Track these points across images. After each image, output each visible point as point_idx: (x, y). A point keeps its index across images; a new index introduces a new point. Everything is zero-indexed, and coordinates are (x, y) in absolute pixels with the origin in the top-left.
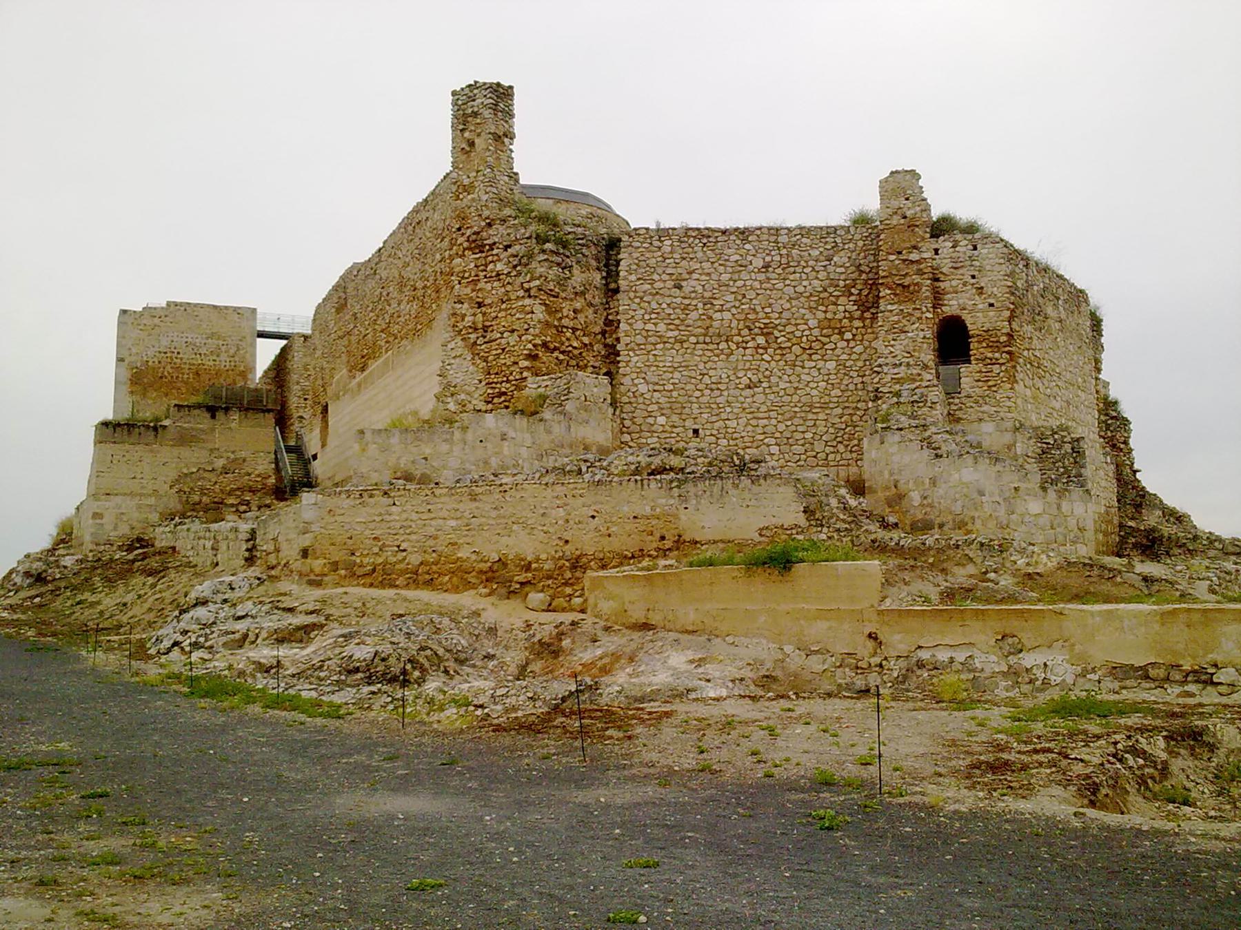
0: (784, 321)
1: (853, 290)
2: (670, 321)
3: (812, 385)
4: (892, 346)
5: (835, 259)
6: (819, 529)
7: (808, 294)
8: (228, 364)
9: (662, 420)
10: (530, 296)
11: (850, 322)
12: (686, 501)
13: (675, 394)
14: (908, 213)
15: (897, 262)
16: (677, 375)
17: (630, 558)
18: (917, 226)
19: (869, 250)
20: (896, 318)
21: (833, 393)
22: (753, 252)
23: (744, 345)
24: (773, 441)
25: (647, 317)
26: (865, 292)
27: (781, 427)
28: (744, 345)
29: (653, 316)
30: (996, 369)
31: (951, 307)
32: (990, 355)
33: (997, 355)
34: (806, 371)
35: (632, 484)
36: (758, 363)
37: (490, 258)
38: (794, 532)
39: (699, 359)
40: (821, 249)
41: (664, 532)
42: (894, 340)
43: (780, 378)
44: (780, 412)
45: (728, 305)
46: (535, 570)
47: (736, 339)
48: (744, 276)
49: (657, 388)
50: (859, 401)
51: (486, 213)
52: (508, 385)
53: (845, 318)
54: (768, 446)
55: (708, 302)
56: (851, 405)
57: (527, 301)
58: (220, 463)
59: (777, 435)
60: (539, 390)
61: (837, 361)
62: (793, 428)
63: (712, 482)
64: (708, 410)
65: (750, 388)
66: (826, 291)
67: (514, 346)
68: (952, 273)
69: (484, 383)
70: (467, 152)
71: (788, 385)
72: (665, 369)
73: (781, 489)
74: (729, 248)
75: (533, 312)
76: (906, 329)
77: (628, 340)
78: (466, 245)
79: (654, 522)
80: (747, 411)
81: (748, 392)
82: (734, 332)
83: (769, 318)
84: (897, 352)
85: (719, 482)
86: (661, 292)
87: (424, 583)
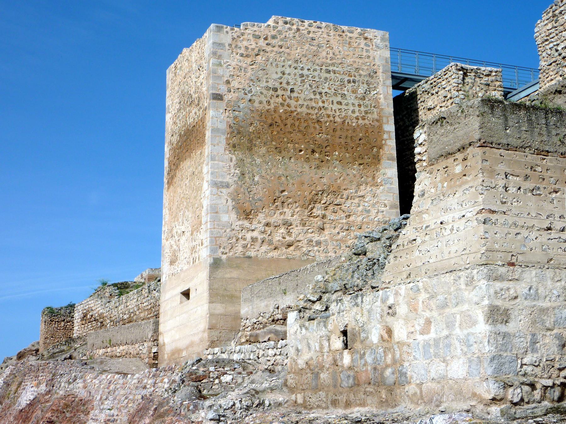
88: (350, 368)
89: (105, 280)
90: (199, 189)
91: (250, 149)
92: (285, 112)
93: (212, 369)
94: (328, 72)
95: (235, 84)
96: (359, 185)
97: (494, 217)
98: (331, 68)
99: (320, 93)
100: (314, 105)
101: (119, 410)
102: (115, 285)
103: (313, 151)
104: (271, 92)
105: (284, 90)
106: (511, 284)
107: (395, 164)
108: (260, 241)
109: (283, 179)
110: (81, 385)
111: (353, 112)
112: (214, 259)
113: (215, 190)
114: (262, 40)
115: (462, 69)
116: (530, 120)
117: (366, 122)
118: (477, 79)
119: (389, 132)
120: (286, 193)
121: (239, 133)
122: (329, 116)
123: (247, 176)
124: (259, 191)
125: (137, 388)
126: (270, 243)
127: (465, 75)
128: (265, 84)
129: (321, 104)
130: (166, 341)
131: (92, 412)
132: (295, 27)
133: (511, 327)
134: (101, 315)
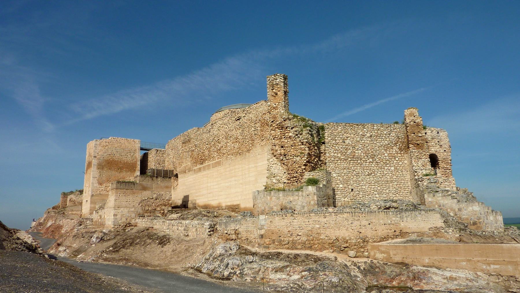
0: (377, 154)
1: (397, 144)
2: (342, 153)
3: (387, 175)
4: (418, 163)
5: (391, 134)
6: (449, 228)
7: (384, 145)
8: (130, 159)
9: (341, 186)
10: (303, 145)
11: (397, 155)
12: (403, 218)
13: (345, 177)
14: (417, 121)
15: (414, 136)
16: (345, 171)
17: (384, 238)
18: (420, 125)
19: (401, 132)
20: (417, 154)
21: (394, 177)
22: (367, 131)
23: (366, 161)
24: (377, 193)
25: (335, 152)
26: (401, 145)
27: (379, 188)
28: (366, 161)
29: (337, 151)
30: (448, 171)
31: (433, 151)
32: (445, 166)
33: (448, 166)
34: (385, 170)
35: (383, 213)
36: (371, 167)
37: (286, 131)
38: (441, 229)
39: (352, 166)
40: (387, 131)
41: (396, 230)
42: (418, 161)
43: (377, 172)
44: (378, 183)
45: (360, 148)
46: (350, 243)
47: (363, 159)
48: (364, 139)
49: (339, 175)
50: (402, 180)
51: (284, 117)
52: (297, 174)
53: (395, 153)
54: (375, 194)
55: (354, 147)
56: (399, 181)
57: (302, 146)
58: (155, 196)
59: (378, 191)
60: (310, 176)
61: (394, 167)
62: (382, 189)
63: (411, 212)
64: (356, 183)
65: (368, 175)
66: (389, 144)
67: (298, 161)
68: (432, 141)
69: (286, 173)
70: (274, 96)
71: (380, 175)
72: (341, 169)
73: (435, 215)
74: (359, 130)
75: (305, 150)
76: (421, 158)
77: (329, 159)
78: (276, 127)
79: (392, 226)
80: (368, 183)
81: (368, 177)
82: (363, 157)
83: (373, 153)
84: (419, 165)
85: (413, 212)
86: (338, 143)
87: (308, 247)
88: (100, 222)
89: (77, 189)
90: (90, 177)
91: (103, 169)
92: (112, 160)
93: (85, 220)
94: (124, 150)
95: (100, 154)
96: (130, 177)
97: (116, 200)
98: (125, 149)
99: (121, 155)
100: (120, 158)
101: (69, 228)
102: (79, 191)
103: (119, 169)
104: (109, 155)
105: (112, 155)
106: (118, 211)
107: (140, 171)
108: (104, 190)
109: (110, 176)
110: (62, 222)
111: (130, 159)
112: (92, 195)
113: (93, 179)
114: (107, 143)
115: (157, 150)
116: (125, 185)
117: (133, 162)
118: (161, 152)
119: (138, 164)
120: (111, 179)
121: (100, 165)
122: (123, 161)
123: (101, 175)
124: (104, 179)
125: (73, 223)
126: (106, 190)
127: (157, 151)
128: (107, 153)
129: (121, 158)
130: (83, 212)
131: (63, 229)
132: (116, 139)
133: (117, 217)
134: (74, 200)
